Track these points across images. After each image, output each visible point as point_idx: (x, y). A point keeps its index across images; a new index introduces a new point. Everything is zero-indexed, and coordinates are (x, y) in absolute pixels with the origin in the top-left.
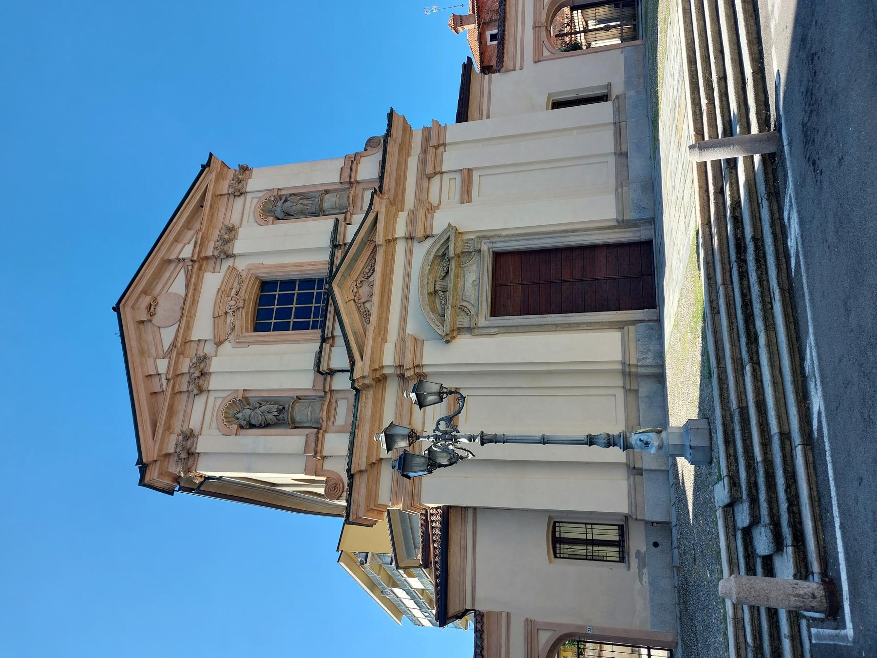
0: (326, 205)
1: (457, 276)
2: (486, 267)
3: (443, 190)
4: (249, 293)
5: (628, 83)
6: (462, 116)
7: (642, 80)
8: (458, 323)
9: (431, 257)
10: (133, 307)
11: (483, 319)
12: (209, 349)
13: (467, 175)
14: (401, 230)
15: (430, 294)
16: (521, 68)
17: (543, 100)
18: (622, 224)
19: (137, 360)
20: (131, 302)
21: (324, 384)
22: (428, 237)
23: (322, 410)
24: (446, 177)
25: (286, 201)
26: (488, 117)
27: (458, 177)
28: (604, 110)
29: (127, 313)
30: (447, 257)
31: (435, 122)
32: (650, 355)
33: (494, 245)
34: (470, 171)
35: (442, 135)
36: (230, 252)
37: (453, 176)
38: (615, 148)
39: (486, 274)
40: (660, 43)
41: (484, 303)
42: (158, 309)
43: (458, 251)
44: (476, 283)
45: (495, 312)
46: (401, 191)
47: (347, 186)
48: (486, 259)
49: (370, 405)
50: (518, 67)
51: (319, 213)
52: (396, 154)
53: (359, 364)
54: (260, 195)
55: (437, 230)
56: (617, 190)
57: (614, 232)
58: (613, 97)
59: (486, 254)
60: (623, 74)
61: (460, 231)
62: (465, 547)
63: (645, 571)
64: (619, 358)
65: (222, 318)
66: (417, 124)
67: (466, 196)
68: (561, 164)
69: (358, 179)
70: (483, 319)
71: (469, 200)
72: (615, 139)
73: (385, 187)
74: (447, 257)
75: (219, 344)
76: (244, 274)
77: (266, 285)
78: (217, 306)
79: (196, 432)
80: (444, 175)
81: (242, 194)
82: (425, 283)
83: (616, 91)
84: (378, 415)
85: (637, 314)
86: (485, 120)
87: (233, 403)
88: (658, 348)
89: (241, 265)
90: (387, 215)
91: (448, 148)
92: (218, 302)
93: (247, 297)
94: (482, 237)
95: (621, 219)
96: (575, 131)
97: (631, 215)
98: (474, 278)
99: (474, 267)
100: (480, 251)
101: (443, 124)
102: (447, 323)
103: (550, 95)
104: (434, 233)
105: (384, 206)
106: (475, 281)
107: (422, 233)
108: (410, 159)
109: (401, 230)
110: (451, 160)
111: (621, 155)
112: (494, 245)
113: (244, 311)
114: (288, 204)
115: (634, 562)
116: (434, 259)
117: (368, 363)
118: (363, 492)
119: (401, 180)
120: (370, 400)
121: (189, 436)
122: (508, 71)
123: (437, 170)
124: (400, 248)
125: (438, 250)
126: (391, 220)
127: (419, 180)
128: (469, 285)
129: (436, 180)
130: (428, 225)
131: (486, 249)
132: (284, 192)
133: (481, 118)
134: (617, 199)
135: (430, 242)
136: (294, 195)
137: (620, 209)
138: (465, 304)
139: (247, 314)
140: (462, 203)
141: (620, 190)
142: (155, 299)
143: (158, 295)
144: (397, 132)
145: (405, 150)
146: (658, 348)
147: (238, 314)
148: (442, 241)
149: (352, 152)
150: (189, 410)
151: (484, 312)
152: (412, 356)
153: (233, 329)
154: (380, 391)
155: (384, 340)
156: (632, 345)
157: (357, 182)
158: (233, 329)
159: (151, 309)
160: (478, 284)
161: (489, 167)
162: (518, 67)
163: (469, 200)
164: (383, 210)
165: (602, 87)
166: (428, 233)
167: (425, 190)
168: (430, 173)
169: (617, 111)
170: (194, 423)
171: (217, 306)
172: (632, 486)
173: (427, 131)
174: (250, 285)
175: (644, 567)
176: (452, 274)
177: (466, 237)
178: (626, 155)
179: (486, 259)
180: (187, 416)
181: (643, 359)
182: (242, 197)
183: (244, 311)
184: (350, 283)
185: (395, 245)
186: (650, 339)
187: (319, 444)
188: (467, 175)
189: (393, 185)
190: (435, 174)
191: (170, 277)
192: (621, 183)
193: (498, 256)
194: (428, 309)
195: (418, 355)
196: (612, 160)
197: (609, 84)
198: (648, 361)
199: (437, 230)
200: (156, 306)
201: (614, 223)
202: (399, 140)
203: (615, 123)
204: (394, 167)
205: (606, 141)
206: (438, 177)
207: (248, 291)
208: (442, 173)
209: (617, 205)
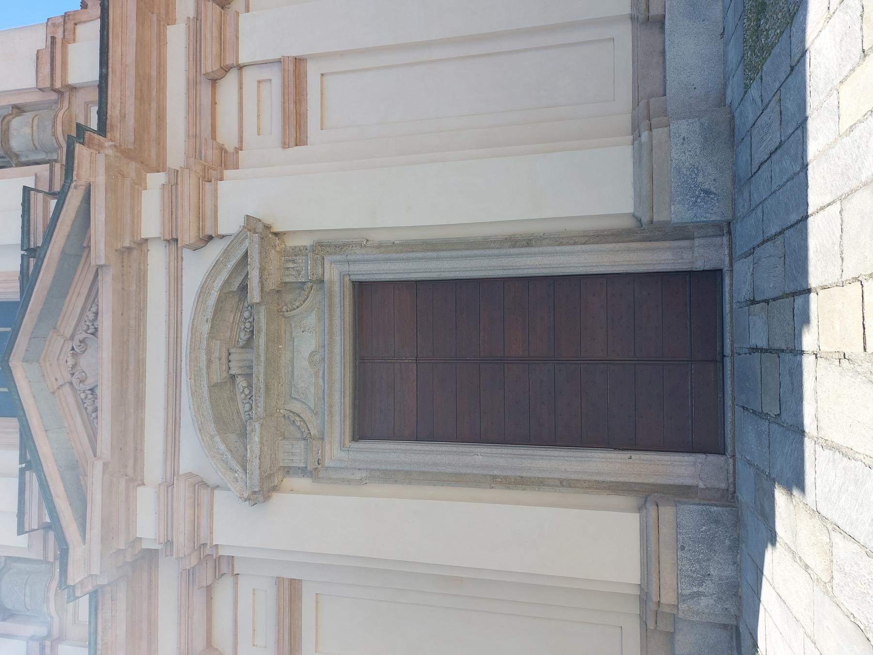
1: (274, 340)
2: (337, 322)
9: (212, 301)
13: (295, 70)
14: (151, 224)
15: (214, 387)
18: (644, 231)
21: (45, 547)
22: (211, 238)
24: (250, 76)
27: (274, 75)
32: (709, 587)
33: (354, 268)
34: (299, 62)
40: (110, 50)
43: (272, 284)
44: (317, 357)
45: (362, 430)
46: (153, 116)
48: (337, 300)
52: (132, 24)
53: (77, 551)
55: (229, 222)
56: (636, 129)
57: (629, 250)
59: (336, 289)
61: (276, 229)
64: (637, 581)
67: (295, 131)
73: (113, 112)
74: (257, 283)
85: (678, 468)
88: (729, 571)
90: (111, 189)
94: (326, 247)
95: (645, 219)
97: (676, 212)
99: (311, 320)
100: (321, 281)
102: (254, 465)
104: (222, 231)
106: (316, 353)
108: (192, 14)
109: (151, 224)
112: (354, 268)
116: (220, 301)
119: (149, 89)
124: (157, 260)
125: (227, 282)
127: (193, 85)
128: (302, 363)
129: (228, 86)
130: (209, 213)
131: (336, 277)
135: (215, 250)
137: (646, 191)
138: (296, 407)
140: (285, 145)
148: (230, 265)
149: (58, 13)
156: (667, 557)
157: (73, 89)
161: (342, 54)
164: (100, 180)
166: (209, 231)
176: (261, 340)
178: (660, 22)
179: (337, 300)
181: (692, 596)
188: (295, 70)
189: (130, 107)
193: (364, 292)
194: (212, 428)
195: (204, 522)
196: (624, 34)
198: (704, 602)
199: (229, 222)
201: (629, 223)
208: (240, 68)
209: (637, 177)
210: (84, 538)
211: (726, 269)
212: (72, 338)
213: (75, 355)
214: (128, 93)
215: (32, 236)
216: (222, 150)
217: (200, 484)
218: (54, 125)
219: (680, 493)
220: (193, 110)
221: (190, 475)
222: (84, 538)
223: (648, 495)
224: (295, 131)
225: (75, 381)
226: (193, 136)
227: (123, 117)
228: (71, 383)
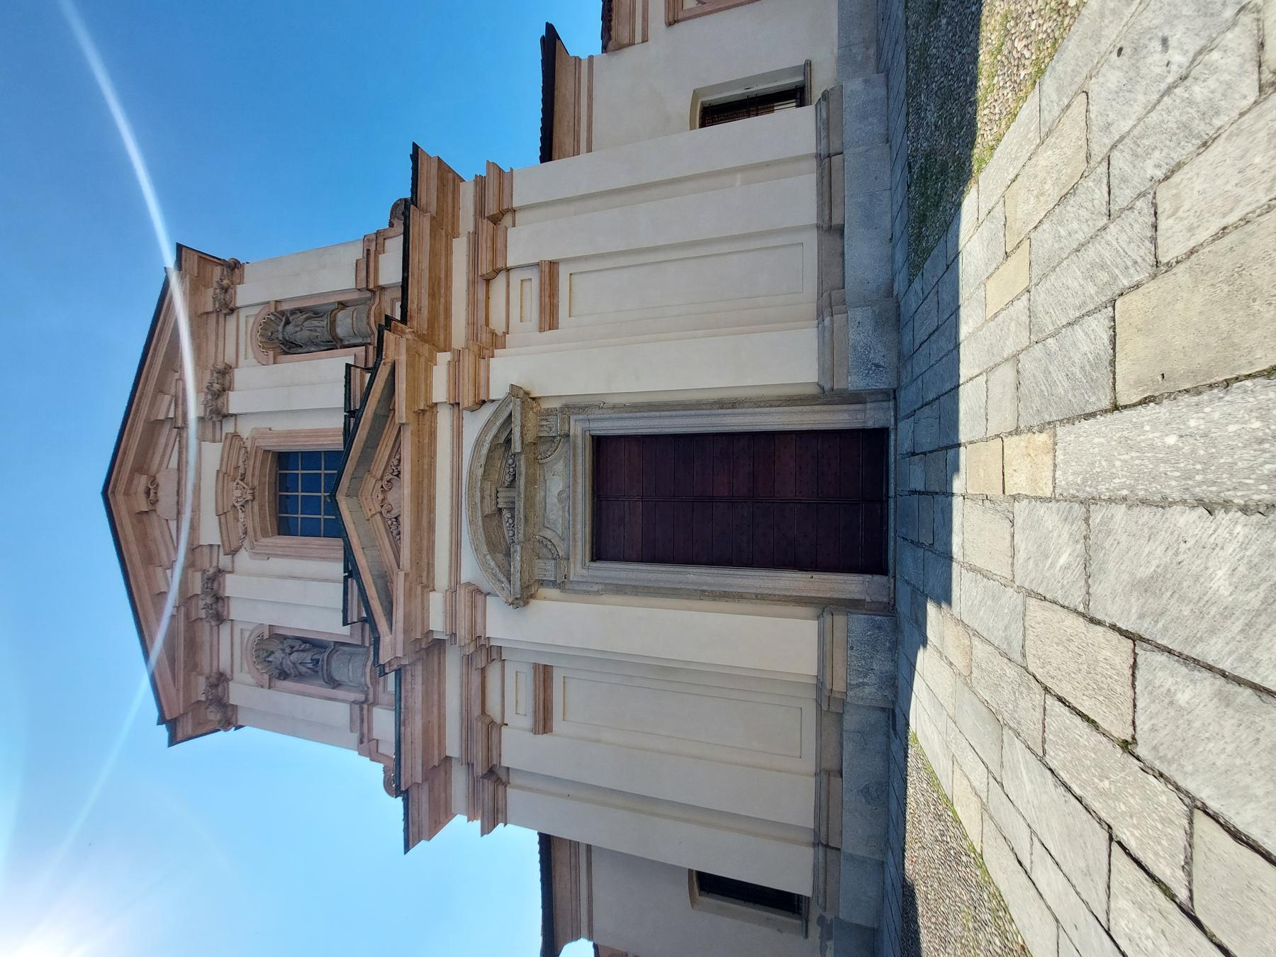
0: (341, 331)
2: (580, 468)
3: (514, 302)
4: (261, 475)
5: (845, 60)
6: (547, 154)
7: (872, 51)
8: (536, 571)
9: (485, 451)
10: (127, 493)
11: (580, 567)
12: (225, 561)
13: (550, 271)
14: (440, 393)
16: (645, 40)
17: (683, 107)
18: (827, 396)
19: (141, 573)
20: (121, 487)
22: (484, 402)
23: (364, 674)
24: (515, 277)
25: (288, 323)
26: (589, 150)
27: (534, 275)
28: (792, 128)
29: (120, 501)
30: (516, 443)
31: (491, 166)
32: (872, 679)
34: (553, 264)
35: (506, 192)
36: (225, 411)
37: (527, 274)
38: (820, 215)
39: (580, 480)
41: (579, 535)
42: (160, 494)
43: (530, 438)
44: (564, 495)
45: (599, 553)
46: (442, 308)
47: (369, 294)
48: (580, 451)
49: (419, 687)
50: (638, 38)
51: (333, 343)
53: (386, 640)
54: (256, 310)
55: (498, 391)
58: (816, 93)
59: (579, 442)
60: (835, 39)
62: (577, 867)
63: (830, 944)
65: (230, 516)
66: (468, 167)
68: (715, 249)
69: (382, 282)
70: (579, 565)
71: (553, 326)
72: (820, 194)
73: (412, 306)
74: (516, 443)
75: (233, 552)
76: (248, 444)
77: (284, 459)
79: (228, 673)
80: (512, 274)
81: (232, 311)
82: (478, 500)
83: (820, 83)
84: (436, 697)
86: (584, 156)
87: (261, 640)
88: (888, 667)
89: (246, 429)
90: (411, 365)
91: (518, 216)
92: (221, 492)
93: (256, 483)
94: (572, 408)
95: (827, 387)
96: (739, 176)
98: (560, 488)
99: (560, 466)
100: (568, 436)
101: (507, 170)
102: (516, 578)
103: (696, 94)
105: (403, 351)
106: (562, 492)
107: (471, 399)
109: (440, 393)
110: (523, 244)
111: (832, 230)
112: (593, 425)
113: (256, 504)
114: (290, 328)
115: (815, 931)
117: (400, 637)
118: (425, 806)
120: (419, 680)
121: (220, 680)
122: (621, 47)
123: (500, 265)
124: (444, 419)
125: (496, 436)
126: (421, 380)
127: (472, 284)
128: (552, 499)
129: (499, 284)
131: (579, 433)
132: (285, 307)
133: (576, 152)
134: (822, 344)
135: (487, 411)
136: (301, 310)
137: (828, 365)
138: (548, 534)
139: (261, 507)
140: (541, 330)
141: (827, 320)
142: (153, 480)
143: (158, 471)
144: (429, 195)
145: (444, 226)
146: (888, 667)
147: (249, 506)
148: (501, 421)
150: (215, 643)
151: (579, 557)
152: (468, 623)
153: (246, 533)
154: (436, 659)
155: (429, 587)
156: (839, 655)
157: (382, 288)
158: (246, 533)
159: (151, 493)
160: (566, 498)
161: (586, 258)
162: (638, 38)
163: (553, 326)
164: (403, 358)
165: (793, 71)
166: (483, 397)
167: (482, 305)
168: (488, 274)
169: (825, 127)
170: (224, 664)
172: (821, 865)
173: (480, 182)
174: (258, 464)
175: (830, 939)
176: (522, 482)
177: (545, 405)
178: (841, 230)
179: (580, 451)
180: (215, 651)
181: (858, 685)
182: (235, 314)
183: (256, 504)
184: (371, 484)
185: (434, 416)
186: (874, 647)
187: (365, 725)
188: (550, 271)
189: (425, 302)
190: (497, 272)
191: (166, 445)
192: (831, 301)
193: (600, 444)
195: (479, 620)
197: (808, 64)
198: (867, 690)
199: (498, 391)
200: (156, 488)
202: (433, 208)
203: (818, 156)
204: (425, 264)
205: (799, 199)
206: (502, 277)
207: (257, 473)
208: (508, 270)
209: (821, 354)
212: (382, 479)
213: (384, 491)
216: (493, 334)
217: (477, 592)
219: (851, 605)
221: (469, 584)
223: (825, 607)
226: (472, 323)
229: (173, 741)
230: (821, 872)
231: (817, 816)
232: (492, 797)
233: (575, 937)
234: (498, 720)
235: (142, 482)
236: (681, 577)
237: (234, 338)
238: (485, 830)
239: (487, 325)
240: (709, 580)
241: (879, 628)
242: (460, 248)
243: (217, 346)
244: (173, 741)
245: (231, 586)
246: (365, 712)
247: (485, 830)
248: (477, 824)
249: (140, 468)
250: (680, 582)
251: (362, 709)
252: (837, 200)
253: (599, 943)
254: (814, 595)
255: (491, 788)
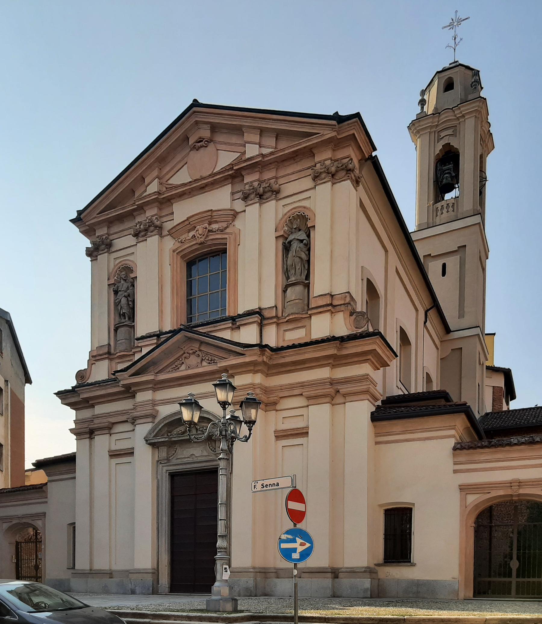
42: (202, 150)
45: (173, 476)
53: (126, 374)
67: (281, 435)
71: (278, 438)
78: (197, 217)
79: (113, 249)
99: (205, 453)
106: (194, 456)
139: (196, 250)
142: (210, 141)
164: (247, 359)
171: (197, 217)
180: (121, 234)
198: (130, 585)
210: (360, 199)
211: (483, 443)
212: (200, 350)
213: (194, 353)
214: (293, 357)
215: (240, 319)
216: (275, 403)
217: (154, 416)
218: (292, 314)
219: (157, 581)
220: (292, 387)
221: (157, 411)
222: (360, 199)
223: (156, 572)
224: (281, 435)
225: (185, 355)
226: (282, 388)
227: (284, 357)
228: (184, 353)
229: (72, 221)
230: (82, 572)
231: (98, 570)
232: (85, 431)
233: (48, 475)
234: (112, 431)
235: (206, 133)
236: (164, 514)
237: (285, 200)
238: (71, 430)
239: (281, 398)
240: (164, 526)
241: (148, 589)
242: (323, 373)
243: (293, 173)
244: (72, 221)
245: (153, 240)
246: (105, 356)
247: (71, 430)
248: (73, 426)
249: (214, 128)
250: (162, 515)
251: (105, 354)
252: (311, 575)
253: (81, 463)
254: (390, 617)
255: (87, 431)
